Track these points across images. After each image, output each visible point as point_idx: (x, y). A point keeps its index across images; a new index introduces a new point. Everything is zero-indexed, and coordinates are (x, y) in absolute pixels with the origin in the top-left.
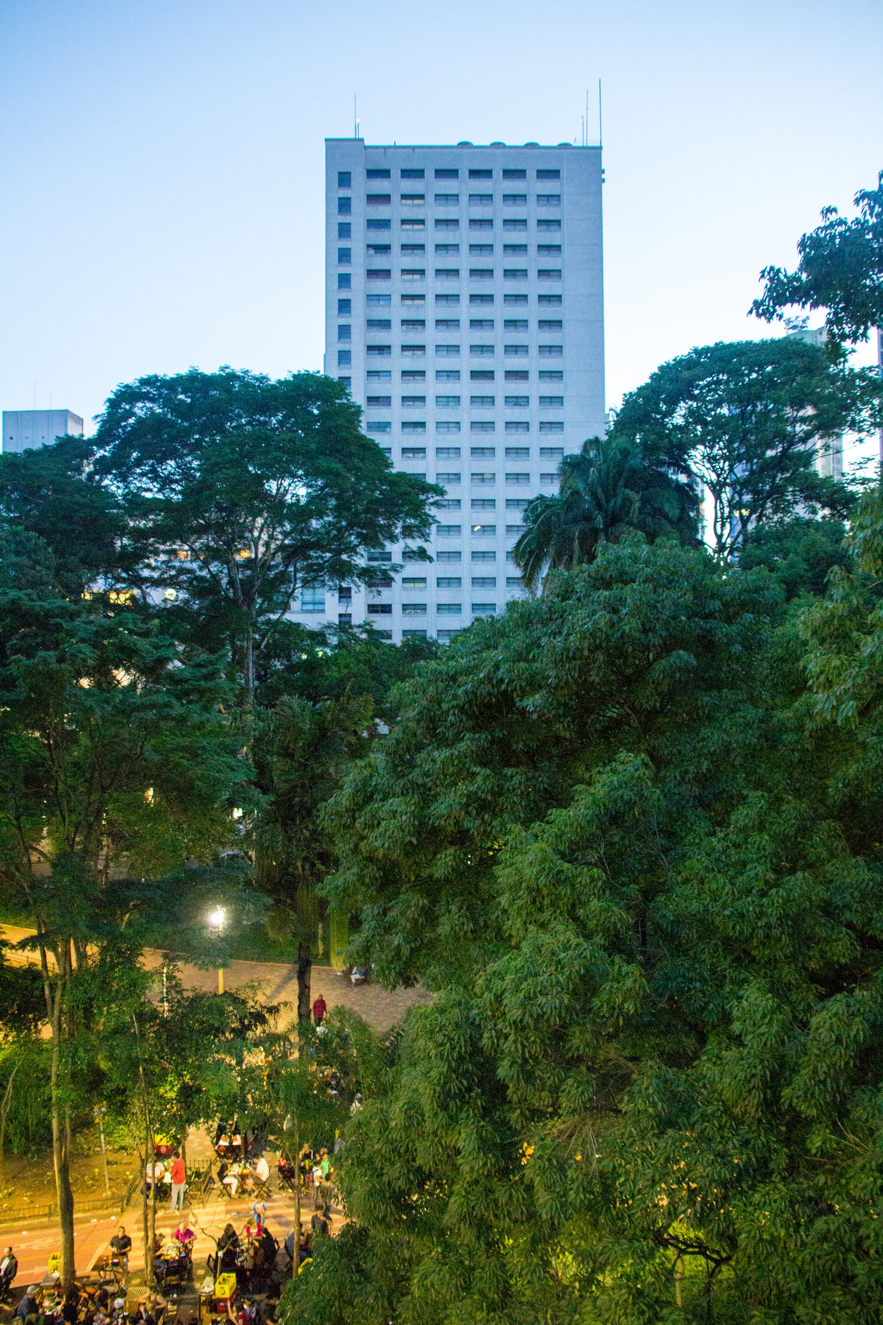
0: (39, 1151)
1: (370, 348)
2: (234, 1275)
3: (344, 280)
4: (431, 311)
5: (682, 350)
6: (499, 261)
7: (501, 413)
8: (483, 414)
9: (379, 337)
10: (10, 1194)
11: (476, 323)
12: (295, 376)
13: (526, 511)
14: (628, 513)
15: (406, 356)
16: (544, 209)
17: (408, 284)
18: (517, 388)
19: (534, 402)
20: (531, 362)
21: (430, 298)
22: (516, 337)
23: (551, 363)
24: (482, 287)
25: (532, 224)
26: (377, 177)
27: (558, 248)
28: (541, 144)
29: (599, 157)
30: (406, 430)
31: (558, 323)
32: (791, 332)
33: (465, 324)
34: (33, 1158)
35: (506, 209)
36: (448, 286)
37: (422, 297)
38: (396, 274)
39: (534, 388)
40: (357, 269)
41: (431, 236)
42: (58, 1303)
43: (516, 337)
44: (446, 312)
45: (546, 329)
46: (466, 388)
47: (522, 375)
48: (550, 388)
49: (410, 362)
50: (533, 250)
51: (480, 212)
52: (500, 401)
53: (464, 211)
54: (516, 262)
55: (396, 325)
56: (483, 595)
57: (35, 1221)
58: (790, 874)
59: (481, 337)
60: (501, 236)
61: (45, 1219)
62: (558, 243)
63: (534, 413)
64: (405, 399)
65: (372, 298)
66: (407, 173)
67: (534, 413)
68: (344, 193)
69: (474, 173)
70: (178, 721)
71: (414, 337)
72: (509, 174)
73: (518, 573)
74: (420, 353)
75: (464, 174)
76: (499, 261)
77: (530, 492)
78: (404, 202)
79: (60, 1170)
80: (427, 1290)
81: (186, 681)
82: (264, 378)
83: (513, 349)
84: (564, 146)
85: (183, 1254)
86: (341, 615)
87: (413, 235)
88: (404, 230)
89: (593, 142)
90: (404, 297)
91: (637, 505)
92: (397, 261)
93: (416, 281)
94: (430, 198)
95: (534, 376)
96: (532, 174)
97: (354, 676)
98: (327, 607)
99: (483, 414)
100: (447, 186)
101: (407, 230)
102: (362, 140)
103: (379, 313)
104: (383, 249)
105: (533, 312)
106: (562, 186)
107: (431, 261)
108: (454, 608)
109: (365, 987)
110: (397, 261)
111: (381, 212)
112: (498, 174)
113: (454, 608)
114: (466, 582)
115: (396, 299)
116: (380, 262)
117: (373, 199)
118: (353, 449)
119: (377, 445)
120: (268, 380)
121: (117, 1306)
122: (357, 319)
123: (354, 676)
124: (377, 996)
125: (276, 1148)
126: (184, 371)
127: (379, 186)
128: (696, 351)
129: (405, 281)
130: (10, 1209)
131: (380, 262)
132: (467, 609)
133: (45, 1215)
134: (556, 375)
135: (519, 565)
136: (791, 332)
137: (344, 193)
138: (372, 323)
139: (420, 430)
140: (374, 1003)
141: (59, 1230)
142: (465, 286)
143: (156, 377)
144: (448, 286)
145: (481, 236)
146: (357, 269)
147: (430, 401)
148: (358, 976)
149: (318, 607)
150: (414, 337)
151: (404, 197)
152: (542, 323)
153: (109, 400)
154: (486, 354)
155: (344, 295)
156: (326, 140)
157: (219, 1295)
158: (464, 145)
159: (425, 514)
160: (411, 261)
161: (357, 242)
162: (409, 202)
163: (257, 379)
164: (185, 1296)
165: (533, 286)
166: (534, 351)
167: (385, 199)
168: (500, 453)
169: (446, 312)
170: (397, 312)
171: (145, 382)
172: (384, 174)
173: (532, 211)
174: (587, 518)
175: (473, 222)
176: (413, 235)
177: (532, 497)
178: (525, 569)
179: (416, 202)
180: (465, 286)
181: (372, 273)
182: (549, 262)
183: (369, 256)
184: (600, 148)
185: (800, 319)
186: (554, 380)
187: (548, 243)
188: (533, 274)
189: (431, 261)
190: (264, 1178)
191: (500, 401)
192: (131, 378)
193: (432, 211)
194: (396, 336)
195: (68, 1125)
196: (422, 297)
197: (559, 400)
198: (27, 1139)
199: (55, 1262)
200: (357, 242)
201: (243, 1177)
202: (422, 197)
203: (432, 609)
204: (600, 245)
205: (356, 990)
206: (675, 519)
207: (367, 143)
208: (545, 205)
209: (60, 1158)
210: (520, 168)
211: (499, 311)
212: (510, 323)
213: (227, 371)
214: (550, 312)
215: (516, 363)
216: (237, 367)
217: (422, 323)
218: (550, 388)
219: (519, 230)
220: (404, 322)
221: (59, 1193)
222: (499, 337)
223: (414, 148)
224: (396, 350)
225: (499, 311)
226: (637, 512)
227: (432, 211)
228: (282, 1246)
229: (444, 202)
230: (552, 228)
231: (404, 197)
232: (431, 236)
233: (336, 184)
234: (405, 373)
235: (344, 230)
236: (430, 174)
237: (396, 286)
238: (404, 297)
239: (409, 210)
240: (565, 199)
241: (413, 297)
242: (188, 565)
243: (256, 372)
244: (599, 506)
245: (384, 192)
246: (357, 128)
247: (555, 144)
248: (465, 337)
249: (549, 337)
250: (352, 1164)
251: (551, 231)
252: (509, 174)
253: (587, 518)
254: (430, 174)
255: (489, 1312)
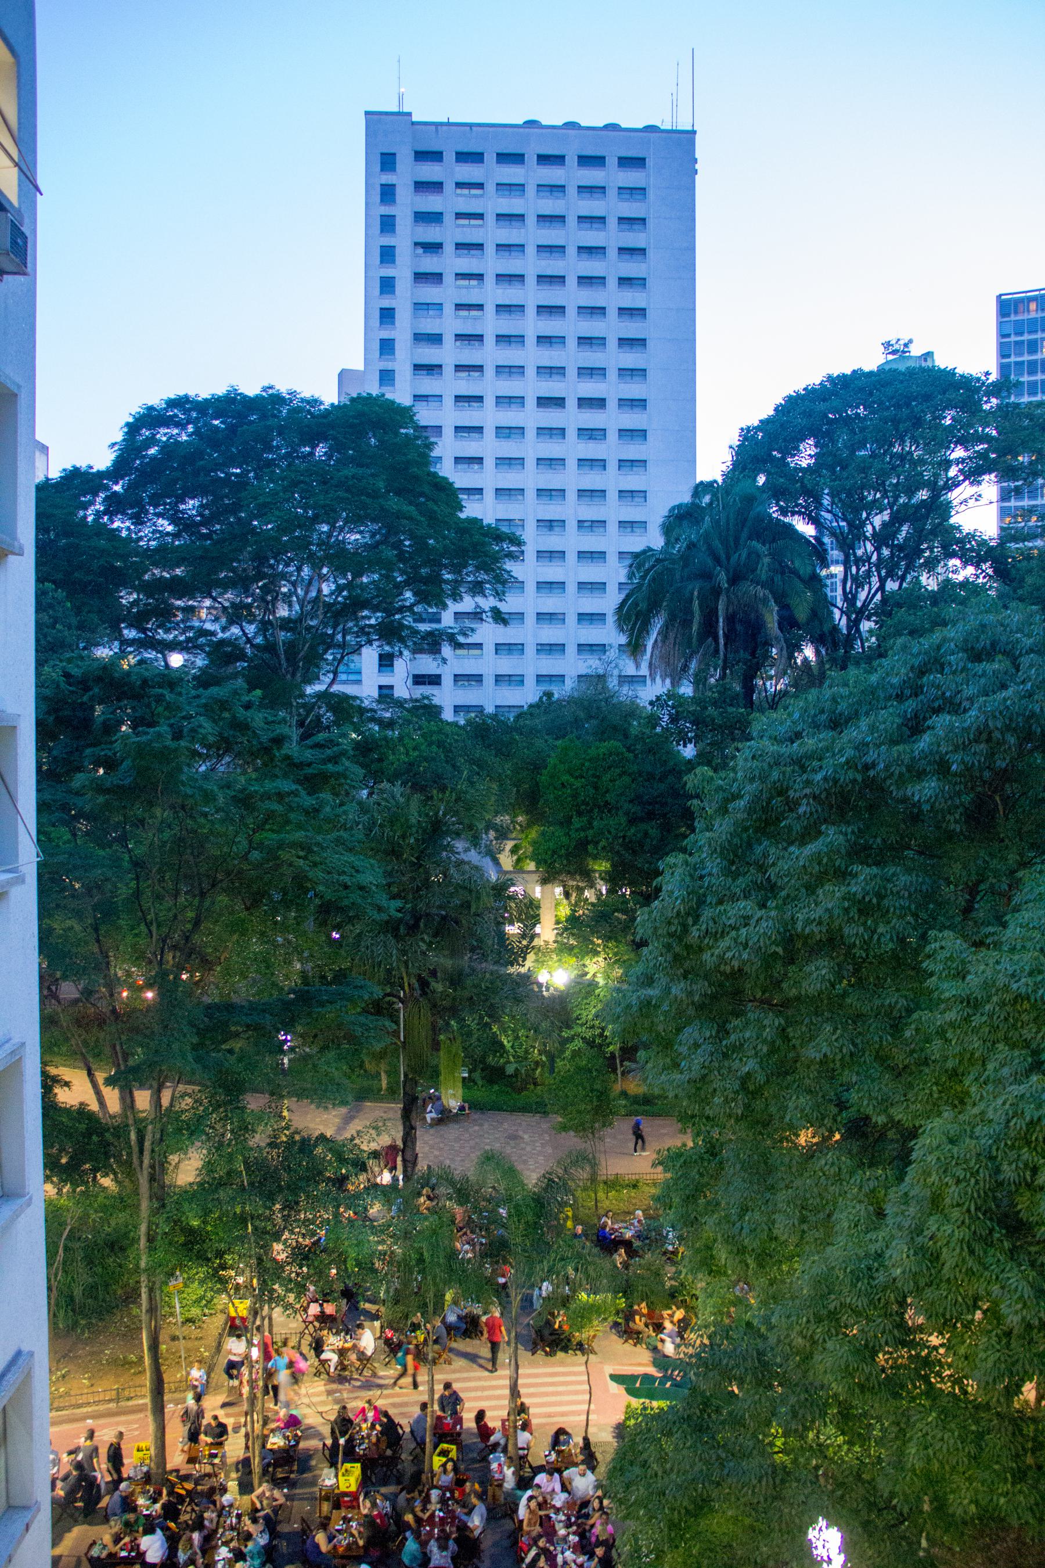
0: (89, 1326)
1: (417, 367)
2: (359, 1465)
3: (387, 285)
4: (490, 324)
5: (813, 376)
6: (573, 266)
7: (573, 448)
8: (552, 449)
9: (429, 354)
10: (64, 1376)
11: (543, 340)
12: (353, 400)
13: (631, 566)
14: (754, 570)
15: (462, 379)
16: (626, 204)
17: (464, 291)
18: (592, 419)
19: (612, 436)
20: (610, 388)
21: (490, 309)
22: (592, 358)
23: (634, 390)
24: (552, 296)
25: (612, 222)
26: (466, 162)
27: (642, 251)
28: (545, 122)
29: (692, 143)
30: (459, 466)
31: (642, 342)
32: (890, 357)
33: (531, 340)
34: (83, 1333)
35: (581, 203)
36: (510, 295)
37: (480, 307)
38: (449, 279)
39: (612, 419)
40: (402, 271)
41: (492, 234)
42: (155, 1501)
43: (592, 358)
44: (508, 325)
45: (627, 348)
46: (531, 417)
47: (599, 403)
48: (632, 420)
49: (465, 386)
50: (612, 253)
51: (550, 206)
52: (571, 434)
53: (532, 204)
54: (592, 267)
55: (449, 339)
56: (549, 665)
57: (102, 1408)
58: (229, 1008)
59: (550, 357)
60: (574, 236)
61: (112, 1405)
62: (643, 246)
63: (611, 449)
64: (458, 429)
65: (419, 307)
66: (463, 157)
67: (611, 449)
68: (387, 178)
69: (544, 159)
70: (307, 813)
71: (470, 355)
72: (584, 160)
73: (623, 639)
74: (477, 374)
75: (531, 159)
76: (573, 266)
77: (636, 543)
78: (459, 191)
79: (150, 1349)
80: (929, 1460)
81: (309, 765)
82: (316, 401)
83: (588, 372)
84: (651, 129)
85: (293, 1443)
86: (380, 687)
87: (470, 233)
88: (458, 226)
89: (685, 125)
90: (459, 307)
91: (767, 560)
92: (450, 263)
93: (474, 287)
94: (490, 188)
95: (612, 404)
96: (612, 161)
97: (426, 759)
98: (364, 677)
99: (552, 449)
100: (511, 173)
101: (463, 226)
102: (410, 114)
103: (429, 326)
104: (433, 248)
105: (612, 327)
106: (648, 176)
107: (491, 264)
108: (515, 680)
109: (439, 1128)
110: (450, 263)
111: (432, 203)
112: (571, 160)
113: (515, 680)
114: (530, 650)
115: (449, 309)
116: (429, 263)
117: (421, 186)
118: (426, 489)
119: (451, 484)
120: (322, 403)
121: (226, 1503)
122: (402, 332)
123: (426, 759)
124: (458, 1139)
125: (375, 1317)
126: (221, 390)
127: (430, 171)
128: (830, 378)
129: (459, 287)
130: (67, 1394)
131: (429, 263)
132: (530, 681)
133: (110, 1401)
134: (638, 404)
135: (622, 630)
136: (890, 357)
137: (387, 178)
138: (419, 338)
139: (476, 467)
140: (457, 1146)
141: (150, 1419)
142: (531, 295)
143: (186, 396)
144: (510, 295)
145: (552, 236)
146: (402, 271)
147: (489, 433)
148: (434, 1115)
149: (352, 677)
150: (470, 355)
151: (459, 185)
152: (623, 342)
153: (128, 424)
154: (555, 377)
155: (386, 303)
156: (367, 113)
157: (343, 1488)
158: (531, 124)
159: (499, 568)
160: (467, 263)
161: (403, 239)
162: (466, 192)
163: (308, 402)
164: (298, 1491)
165: (612, 297)
166: (612, 375)
167: (436, 187)
168: (571, 496)
169: (508, 325)
170: (450, 324)
171: (172, 403)
172: (436, 156)
173: (612, 207)
174: (707, 575)
175: (541, 218)
176: (470, 233)
177: (638, 548)
178: (631, 636)
179: (474, 192)
180: (531, 295)
181: (420, 277)
182: (632, 268)
183: (417, 256)
184: (694, 132)
185: (902, 342)
186: (636, 410)
187: (631, 246)
188: (612, 283)
189: (491, 264)
190: (369, 1353)
191: (571, 434)
192: (156, 398)
193: (493, 204)
194: (448, 354)
195: (144, 1296)
196: (480, 307)
197: (642, 434)
198: (73, 1310)
199: (141, 1454)
200: (403, 239)
201: (342, 1352)
202: (480, 186)
203: (489, 681)
204: (692, 249)
205: (432, 1131)
206: (807, 577)
207: (414, 119)
208: (627, 200)
209: (149, 1331)
210: (599, 154)
211: (571, 326)
212: (584, 341)
213: (270, 391)
214: (632, 329)
215: (590, 388)
216: (283, 388)
217: (480, 338)
218: (632, 420)
219: (597, 229)
220: (459, 337)
221: (148, 1374)
222: (571, 357)
223: (471, 126)
224: (448, 370)
225: (571, 326)
226: (765, 568)
227: (493, 204)
228: (408, 1430)
229: (588, 195)
230: (636, 227)
231: (459, 185)
232: (492, 234)
233: (378, 167)
234: (458, 398)
235: (388, 224)
236: (490, 158)
237: (449, 293)
238: (459, 307)
239: (465, 202)
240: (651, 194)
241: (469, 307)
242: (208, 626)
243: (306, 394)
244: (717, 560)
245: (435, 179)
246: (401, 98)
247: (640, 126)
248: (531, 356)
249: (631, 359)
250: (808, 1321)
251: (634, 231)
252: (584, 160)
253: (707, 575)
254: (490, 158)
255: (1013, 1484)
